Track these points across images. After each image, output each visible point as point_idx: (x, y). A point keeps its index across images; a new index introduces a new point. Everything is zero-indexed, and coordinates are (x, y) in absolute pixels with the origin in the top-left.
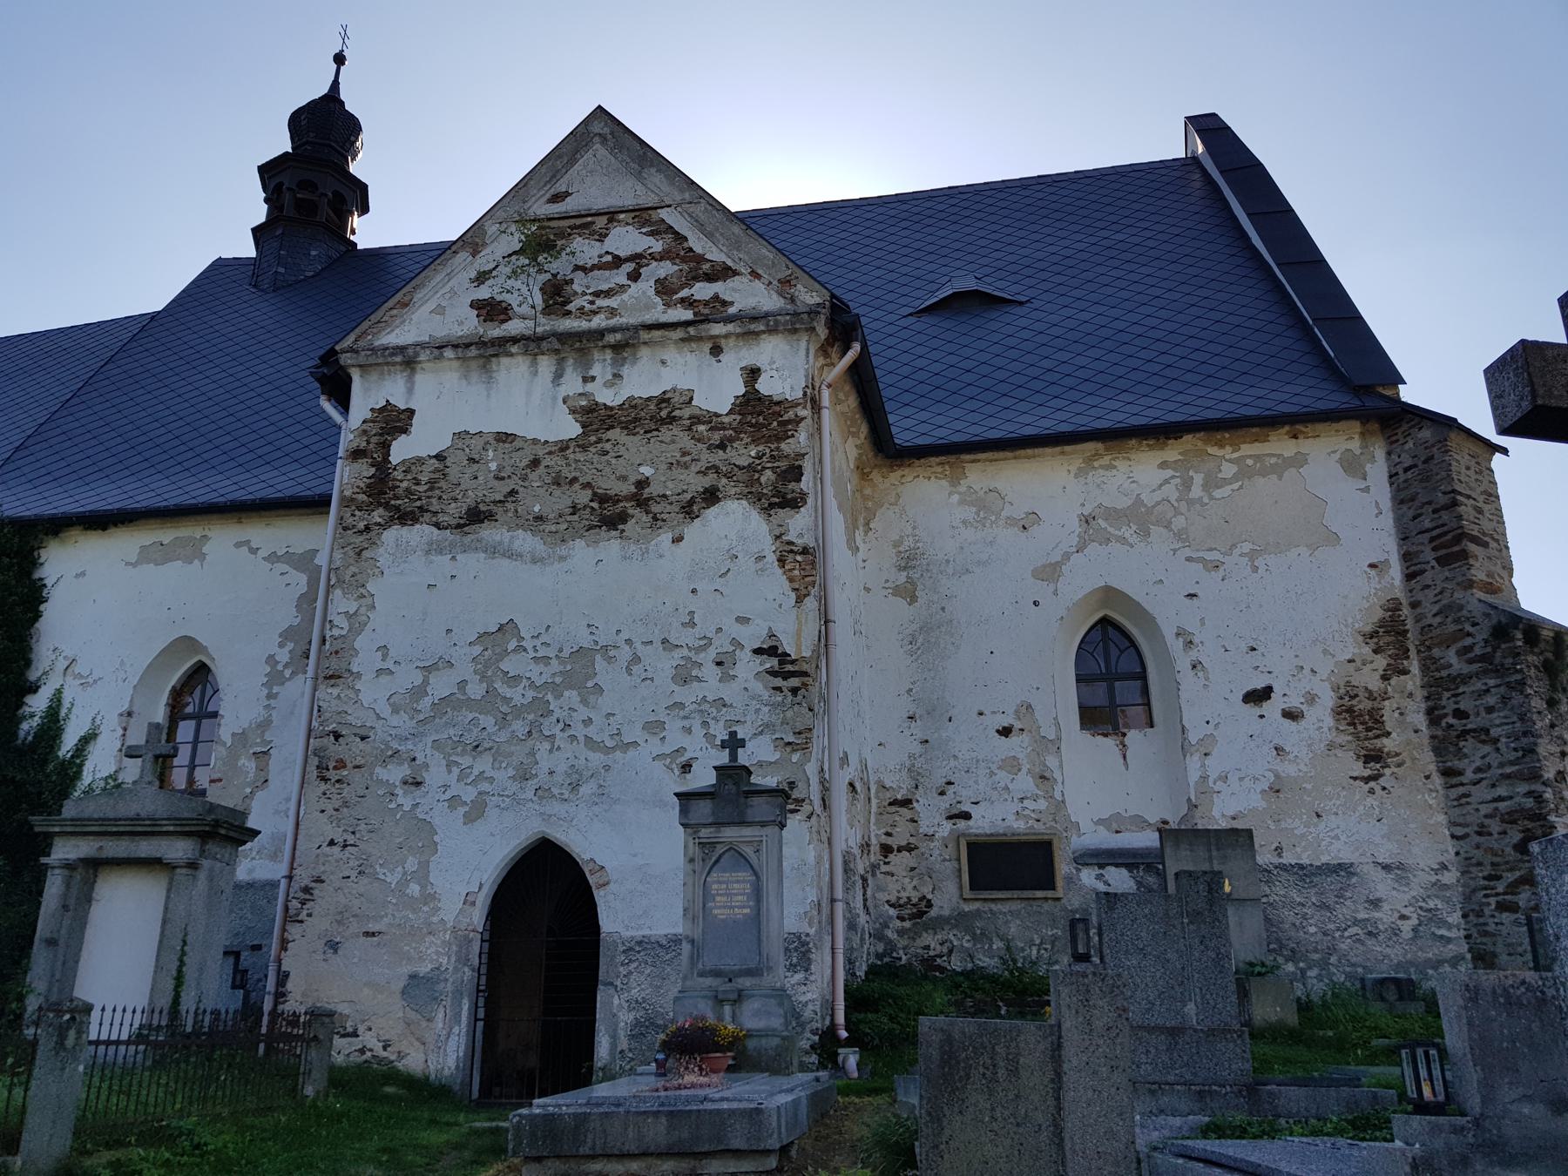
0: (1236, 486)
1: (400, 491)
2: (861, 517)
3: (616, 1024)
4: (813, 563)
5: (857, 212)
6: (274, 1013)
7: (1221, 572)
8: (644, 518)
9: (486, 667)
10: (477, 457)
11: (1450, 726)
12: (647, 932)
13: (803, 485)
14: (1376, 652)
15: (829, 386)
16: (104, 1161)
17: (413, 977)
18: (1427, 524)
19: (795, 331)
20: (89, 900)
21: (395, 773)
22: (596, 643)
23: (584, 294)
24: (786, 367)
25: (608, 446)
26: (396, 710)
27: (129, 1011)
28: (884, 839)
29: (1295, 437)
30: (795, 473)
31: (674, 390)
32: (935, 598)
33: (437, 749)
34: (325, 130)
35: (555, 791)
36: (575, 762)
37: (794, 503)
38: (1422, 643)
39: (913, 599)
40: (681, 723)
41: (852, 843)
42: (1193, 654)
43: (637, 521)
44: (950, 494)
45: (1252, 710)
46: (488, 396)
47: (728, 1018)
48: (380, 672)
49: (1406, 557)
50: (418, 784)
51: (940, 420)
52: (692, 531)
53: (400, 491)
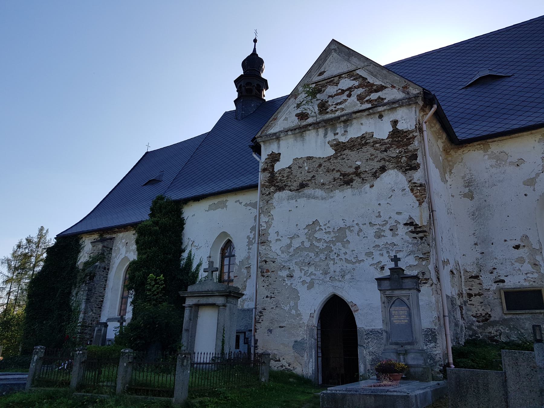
1: (278, 180)
2: (446, 169)
3: (365, 360)
4: (425, 190)
5: (439, 54)
6: (255, 354)
9: (310, 237)
10: (301, 166)
12: (374, 328)
13: (418, 161)
15: (426, 123)
16: (197, 401)
17: (296, 342)
19: (410, 105)
20: (197, 317)
21: (284, 273)
22: (346, 225)
23: (333, 105)
24: (407, 119)
25: (344, 156)
26: (283, 252)
27: (203, 354)
28: (468, 291)
30: (415, 157)
31: (366, 133)
32: (482, 197)
34: (253, 64)
35: (337, 278)
36: (342, 268)
37: (415, 168)
39: (472, 198)
41: (454, 293)
43: (357, 181)
44: (484, 156)
47: (402, 360)
48: (277, 240)
50: (292, 277)
51: (478, 127)
52: (377, 183)
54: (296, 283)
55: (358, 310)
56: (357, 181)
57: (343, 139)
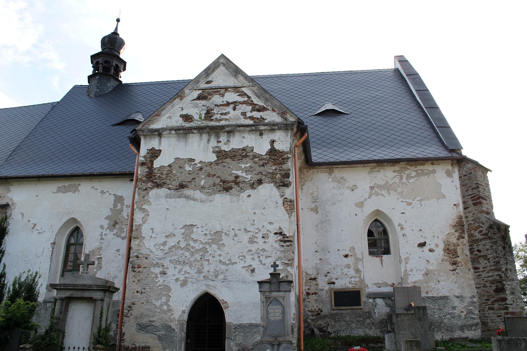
0: (416, 179)
1: (157, 177)
7: (411, 206)
8: (238, 188)
10: (182, 166)
11: (476, 254)
12: (241, 322)
13: (290, 179)
14: (456, 231)
18: (470, 193)
19: (287, 129)
21: (157, 270)
23: (217, 114)
25: (225, 164)
28: (307, 291)
29: (433, 164)
30: (287, 175)
31: (247, 146)
33: (171, 263)
34: (112, 43)
35: (210, 277)
36: (216, 268)
37: (287, 185)
38: (468, 229)
39: (317, 212)
40: (251, 257)
42: (403, 232)
44: (329, 178)
45: (420, 249)
46: (186, 146)
49: (464, 202)
50: (165, 274)
53: (157, 177)
54: (170, 280)
55: (228, 307)
56: (236, 188)
57: (226, 148)
